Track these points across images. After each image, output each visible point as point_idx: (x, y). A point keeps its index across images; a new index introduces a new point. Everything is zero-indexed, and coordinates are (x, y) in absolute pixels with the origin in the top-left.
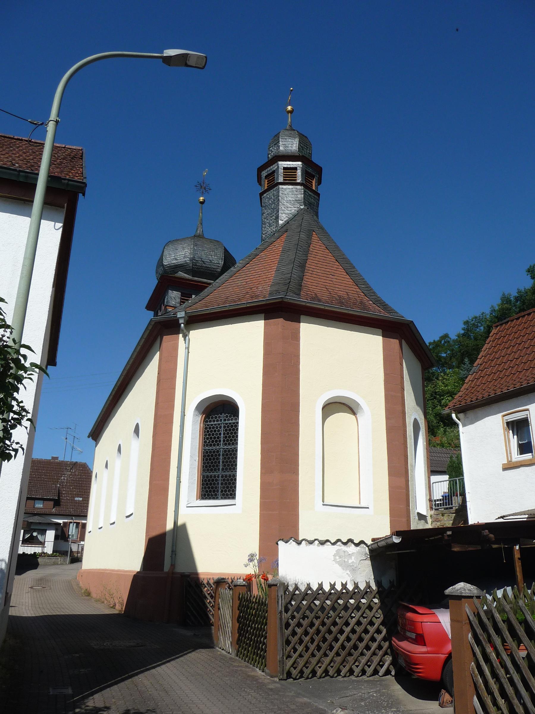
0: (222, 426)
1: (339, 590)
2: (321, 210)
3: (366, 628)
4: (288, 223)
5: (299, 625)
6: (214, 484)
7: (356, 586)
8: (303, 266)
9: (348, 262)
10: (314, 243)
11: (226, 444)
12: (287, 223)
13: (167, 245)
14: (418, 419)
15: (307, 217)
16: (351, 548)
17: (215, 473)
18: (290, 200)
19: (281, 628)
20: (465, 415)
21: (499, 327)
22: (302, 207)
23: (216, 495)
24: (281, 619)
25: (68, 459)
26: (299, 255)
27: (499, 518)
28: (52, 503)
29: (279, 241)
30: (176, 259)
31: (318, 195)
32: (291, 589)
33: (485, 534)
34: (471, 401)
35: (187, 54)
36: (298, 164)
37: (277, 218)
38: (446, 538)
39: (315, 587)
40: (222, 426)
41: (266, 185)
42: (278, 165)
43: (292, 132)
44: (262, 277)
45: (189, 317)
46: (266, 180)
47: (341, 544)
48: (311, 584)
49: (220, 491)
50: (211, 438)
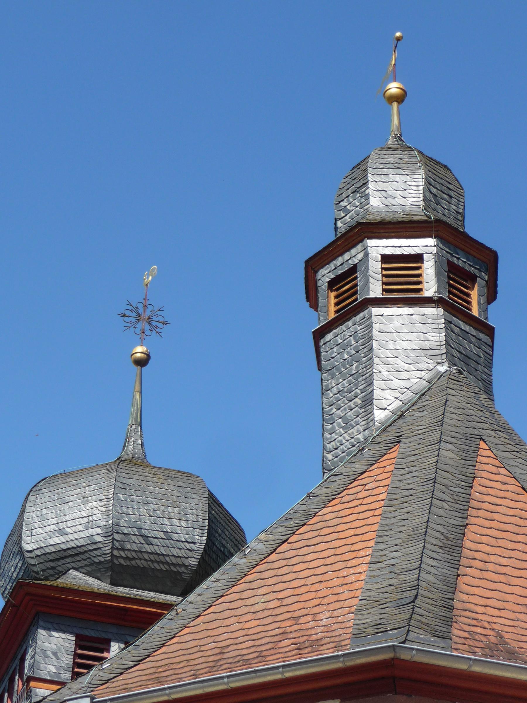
4: (401, 416)
8: (453, 547)
15: (458, 398)
18: (405, 346)
26: (441, 512)
29: (376, 470)
30: (62, 532)
31: (490, 331)
36: (425, 245)
37: (368, 401)
41: (332, 309)
42: (365, 249)
43: (405, 155)
46: (333, 294)
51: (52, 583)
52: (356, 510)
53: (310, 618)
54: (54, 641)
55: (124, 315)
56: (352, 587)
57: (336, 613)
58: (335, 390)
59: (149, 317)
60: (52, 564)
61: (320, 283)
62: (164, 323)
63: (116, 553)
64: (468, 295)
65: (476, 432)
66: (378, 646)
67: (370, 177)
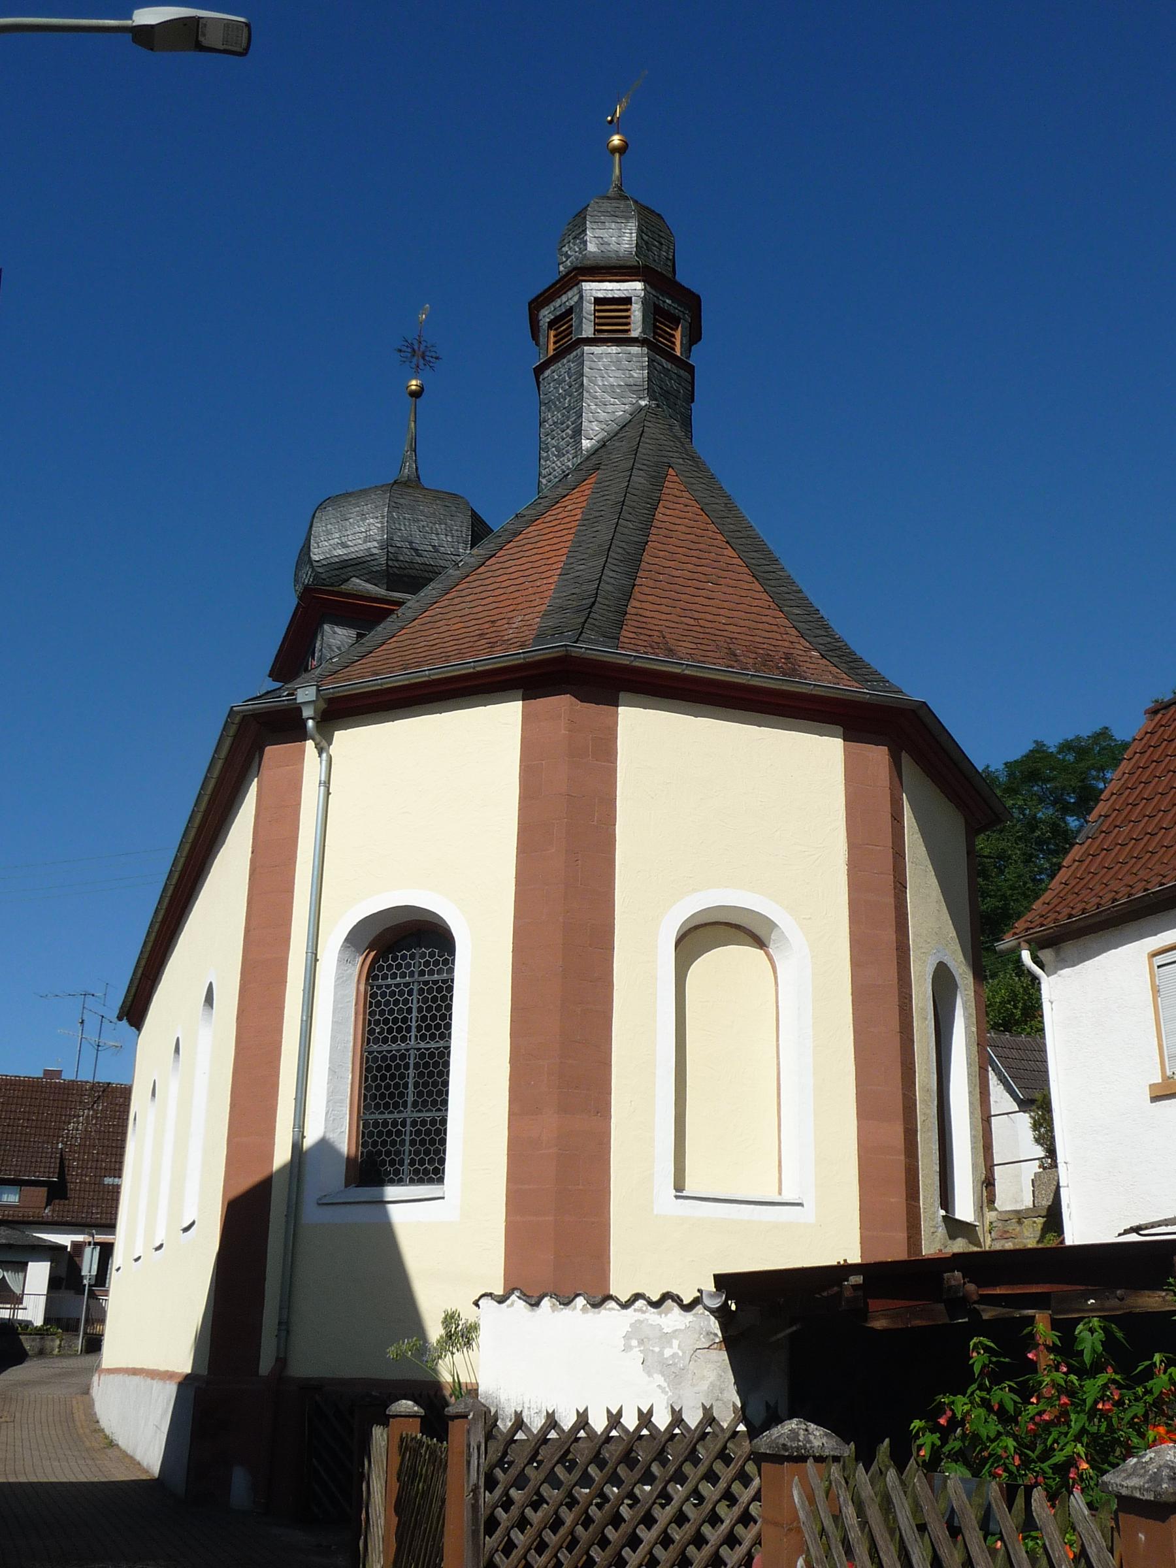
0: (415, 988)
1: (631, 1430)
2: (698, 409)
3: (698, 1531)
4: (604, 445)
5: (522, 1523)
6: (394, 1143)
7: (677, 1419)
8: (634, 563)
9: (761, 548)
10: (670, 498)
11: (423, 1037)
12: (603, 445)
13: (320, 507)
14: (952, 965)
15: (653, 430)
16: (674, 1318)
17: (396, 1115)
18: (611, 384)
19: (475, 1533)
20: (1057, 954)
21: (1160, 715)
22: (643, 403)
23: (397, 1172)
24: (475, 1507)
25: (85, 1076)
26: (626, 531)
27: (1126, 1232)
28: (43, 1191)
29: (576, 493)
30: (344, 545)
31: (691, 369)
32: (505, 1425)
33: (953, 1283)
34: (1070, 916)
35: (196, 20)
36: (635, 288)
37: (578, 432)
38: (848, 1294)
39: (567, 1421)
40: (415, 988)
41: (551, 347)
42: (580, 291)
43: (622, 204)
44: (525, 593)
45: (331, 701)
46: (552, 333)
47: (618, 1307)
48: (524, 1414)
49: (407, 1161)
50: (386, 1021)
51: (335, 589)
52: (556, 529)
53: (505, 621)
54: (339, 637)
55: (400, 351)
56: (542, 595)
57: (527, 618)
58: (550, 422)
59: (423, 353)
60: (337, 572)
61: (541, 323)
62: (437, 358)
63: (390, 563)
64: (673, 336)
65: (666, 460)
66: (552, 648)
67: (588, 224)
